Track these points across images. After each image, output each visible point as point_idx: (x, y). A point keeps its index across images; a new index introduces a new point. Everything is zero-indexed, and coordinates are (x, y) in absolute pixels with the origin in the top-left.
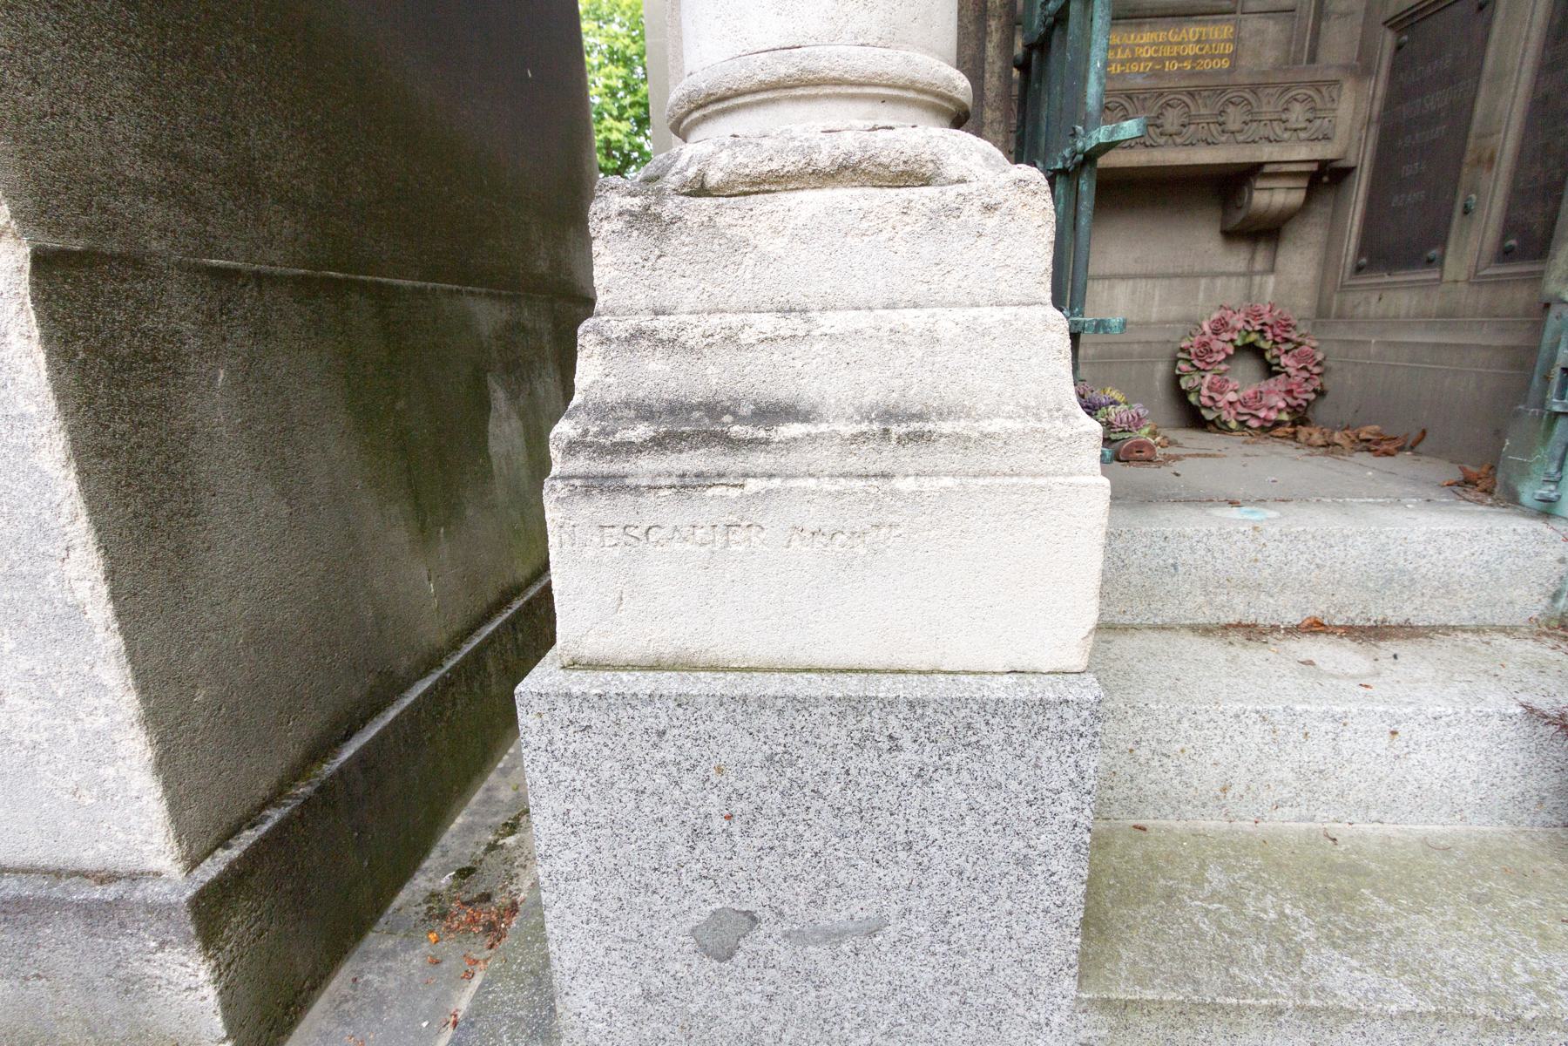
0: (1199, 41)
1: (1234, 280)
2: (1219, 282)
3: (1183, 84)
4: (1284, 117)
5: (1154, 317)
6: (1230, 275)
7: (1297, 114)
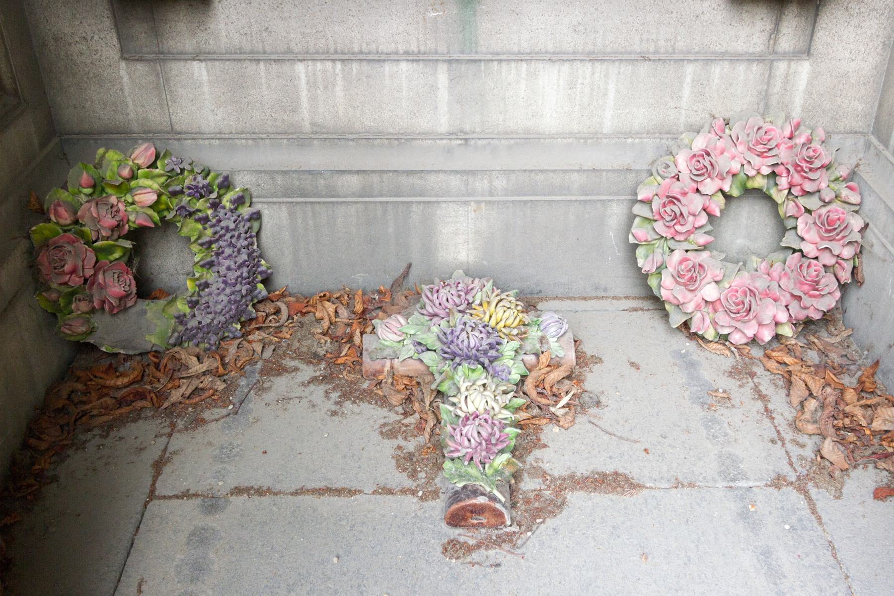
1: (741, 68)
2: (717, 70)
5: (608, 125)
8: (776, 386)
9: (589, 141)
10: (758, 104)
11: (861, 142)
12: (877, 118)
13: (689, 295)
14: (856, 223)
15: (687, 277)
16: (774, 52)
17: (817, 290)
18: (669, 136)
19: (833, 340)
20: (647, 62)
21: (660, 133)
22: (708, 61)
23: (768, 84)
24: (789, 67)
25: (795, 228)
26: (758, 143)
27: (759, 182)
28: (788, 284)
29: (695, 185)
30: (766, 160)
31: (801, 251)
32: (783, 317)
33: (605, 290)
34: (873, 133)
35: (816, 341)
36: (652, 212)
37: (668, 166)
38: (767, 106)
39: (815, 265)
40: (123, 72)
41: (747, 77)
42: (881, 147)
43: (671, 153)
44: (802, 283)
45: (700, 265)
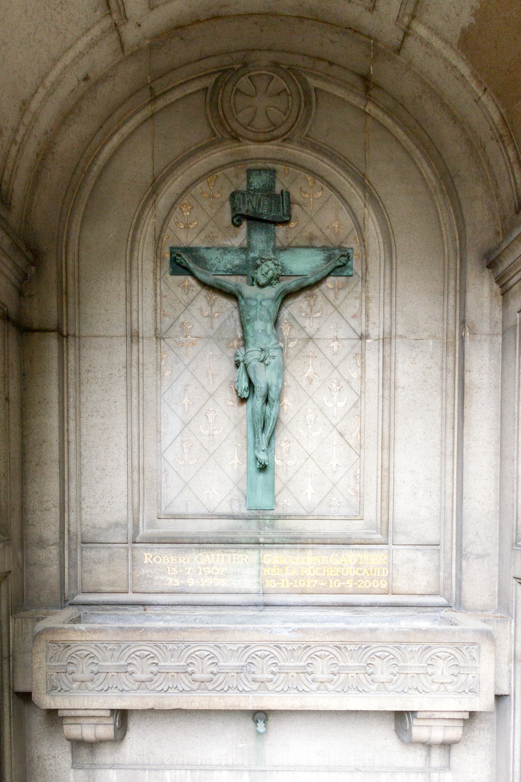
0: (357, 565)
3: (328, 638)
4: (430, 670)
16: (430, 767)
40: (71, 775)
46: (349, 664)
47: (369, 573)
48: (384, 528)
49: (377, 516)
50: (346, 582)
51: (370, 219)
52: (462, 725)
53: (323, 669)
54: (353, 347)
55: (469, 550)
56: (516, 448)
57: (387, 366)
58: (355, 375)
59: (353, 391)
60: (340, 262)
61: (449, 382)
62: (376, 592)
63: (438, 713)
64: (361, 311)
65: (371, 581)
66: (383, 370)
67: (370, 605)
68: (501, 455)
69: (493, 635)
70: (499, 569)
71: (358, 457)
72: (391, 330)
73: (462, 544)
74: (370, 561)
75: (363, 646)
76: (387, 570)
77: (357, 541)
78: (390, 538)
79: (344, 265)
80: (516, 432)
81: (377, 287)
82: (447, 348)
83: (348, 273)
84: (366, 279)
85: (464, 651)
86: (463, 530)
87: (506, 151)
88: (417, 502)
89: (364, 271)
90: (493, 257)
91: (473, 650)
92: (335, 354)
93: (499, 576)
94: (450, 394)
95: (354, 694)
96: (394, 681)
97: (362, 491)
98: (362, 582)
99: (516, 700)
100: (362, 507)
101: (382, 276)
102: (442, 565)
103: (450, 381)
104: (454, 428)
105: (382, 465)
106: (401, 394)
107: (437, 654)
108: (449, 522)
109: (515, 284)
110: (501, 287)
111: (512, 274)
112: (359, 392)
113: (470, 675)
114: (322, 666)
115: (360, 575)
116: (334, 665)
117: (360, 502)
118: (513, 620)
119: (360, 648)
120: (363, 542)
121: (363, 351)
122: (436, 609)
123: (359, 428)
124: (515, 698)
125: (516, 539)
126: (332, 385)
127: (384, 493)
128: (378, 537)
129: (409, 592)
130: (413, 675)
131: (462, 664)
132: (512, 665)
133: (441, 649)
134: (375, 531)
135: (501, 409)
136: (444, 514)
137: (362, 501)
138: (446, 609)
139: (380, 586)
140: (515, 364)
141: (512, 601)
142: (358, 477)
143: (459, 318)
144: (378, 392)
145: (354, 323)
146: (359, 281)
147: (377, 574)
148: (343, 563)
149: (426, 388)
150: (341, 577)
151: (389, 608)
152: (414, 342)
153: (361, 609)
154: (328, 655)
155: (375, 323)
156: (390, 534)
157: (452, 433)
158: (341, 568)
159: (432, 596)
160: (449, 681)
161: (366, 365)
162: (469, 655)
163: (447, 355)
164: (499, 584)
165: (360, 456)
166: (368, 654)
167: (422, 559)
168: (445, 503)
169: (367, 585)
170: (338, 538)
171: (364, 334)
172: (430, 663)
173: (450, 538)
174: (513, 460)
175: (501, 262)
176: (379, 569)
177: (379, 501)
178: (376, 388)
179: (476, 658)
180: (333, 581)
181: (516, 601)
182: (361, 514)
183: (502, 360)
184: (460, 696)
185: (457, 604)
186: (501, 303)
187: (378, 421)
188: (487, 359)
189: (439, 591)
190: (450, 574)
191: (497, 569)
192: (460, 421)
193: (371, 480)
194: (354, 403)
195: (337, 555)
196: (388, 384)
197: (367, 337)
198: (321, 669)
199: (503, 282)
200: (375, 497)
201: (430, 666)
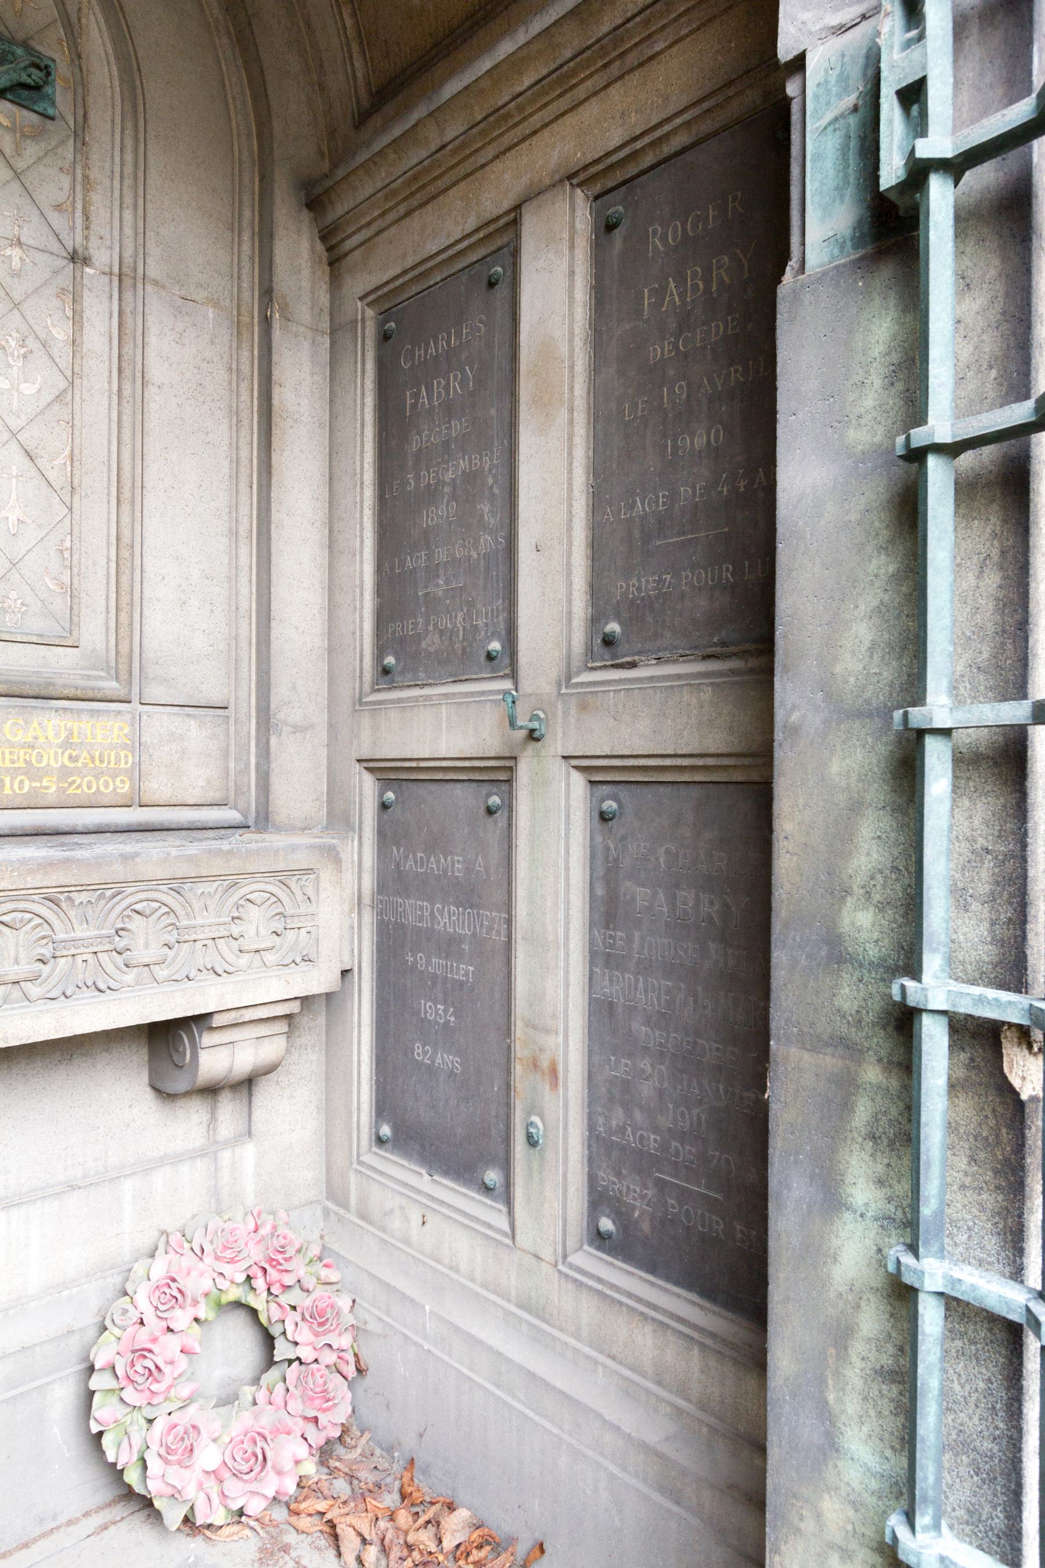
0: (67, 744)
1: (185, 1168)
2: (158, 1178)
3: (31, 881)
4: (235, 930)
6: (175, 1159)
7: (256, 925)
8: (319, 1549)
9: (11, 1312)
10: (209, 1203)
11: (319, 1212)
12: (328, 1182)
13: (186, 1473)
14: (344, 1302)
15: (180, 1451)
16: (216, 1142)
17: (328, 1400)
18: (113, 1271)
19: (355, 1454)
20: (76, 1191)
21: (102, 1271)
22: (147, 1171)
23: (216, 1176)
24: (234, 1154)
25: (284, 1333)
26: (225, 1248)
27: (234, 1294)
28: (296, 1406)
29: (164, 1324)
30: (237, 1265)
31: (298, 1359)
32: (302, 1451)
33: (55, 1517)
34: (327, 1199)
35: (337, 1464)
36: (117, 1378)
37: (125, 1311)
38: (218, 1202)
39: (318, 1370)
41: (192, 1176)
42: (342, 1211)
43: (126, 1294)
44: (312, 1399)
45: (194, 1427)
46: (78, 934)
47: (93, 762)
48: (123, 668)
49: (108, 641)
50: (41, 782)
51: (92, 17)
52: (286, 1029)
53: (18, 953)
54: (56, 273)
55: (281, 716)
56: (358, 534)
57: (127, 334)
58: (61, 333)
59: (55, 368)
60: (29, 76)
61: (243, 399)
62: (106, 801)
63: (250, 1010)
64: (74, 201)
65: (97, 779)
66: (120, 339)
67: (95, 829)
68: (329, 548)
69: (338, 853)
70: (329, 752)
71: (66, 510)
72: (135, 262)
73: (269, 705)
74: (94, 736)
75: (109, 893)
76: (130, 755)
77: (66, 692)
78: (135, 690)
79: (37, 88)
80: (358, 506)
81: (108, 165)
82: (238, 332)
83: (45, 109)
84: (84, 139)
85: (293, 886)
86: (272, 678)
87: (341, 14)
88: (188, 620)
89: (80, 120)
90: (318, 190)
91: (307, 884)
92: (16, 274)
93: (329, 765)
94: (246, 422)
95: (88, 998)
96: (169, 960)
97: (76, 585)
98: (78, 781)
99: (363, 975)
100: (75, 619)
101: (117, 149)
102: (232, 748)
103: (245, 396)
104: (251, 487)
105: (118, 536)
106: (156, 400)
107: (248, 897)
108: (245, 664)
109: (354, 249)
110: (327, 250)
111: (350, 231)
112: (69, 373)
113: (302, 930)
114: (17, 945)
115: (73, 765)
116: (45, 941)
117: (71, 608)
118: (356, 837)
119: (101, 897)
120: (79, 693)
121: (78, 288)
122: (223, 832)
123: (69, 448)
124: (360, 972)
125: (361, 692)
126: (7, 342)
127: (123, 593)
128: (111, 686)
129: (173, 801)
130: (206, 942)
131: (290, 911)
132: (355, 915)
133: (254, 887)
134: (103, 674)
135: (330, 467)
136: (236, 649)
137: (75, 607)
138: (241, 831)
139: (115, 789)
140: (356, 387)
141: (355, 801)
142: (67, 554)
143: (260, 283)
144: (109, 383)
145: (58, 221)
146: (69, 137)
147: (109, 763)
148: (36, 738)
149: (202, 398)
150: (30, 771)
151: (133, 835)
152: (180, 302)
153: (75, 840)
154: (30, 920)
155: (101, 238)
156: (136, 681)
157: (249, 495)
158: (30, 751)
159: (216, 807)
160: (269, 945)
161: (85, 319)
162: (301, 893)
163: (239, 347)
164: (328, 778)
165: (71, 509)
166: (118, 909)
167: (197, 734)
168: (237, 628)
169: (89, 788)
170: (24, 683)
171: (80, 250)
172: (236, 914)
173: (246, 695)
174: (355, 555)
175: (332, 203)
176: (113, 753)
177: (113, 610)
178: (106, 374)
179: (312, 898)
180: (12, 779)
181: (361, 801)
182: (75, 633)
183: (331, 379)
184: (286, 970)
185: (263, 819)
186: (327, 279)
187: (109, 442)
188: (308, 371)
189: (227, 798)
190: (247, 765)
191: (324, 752)
192: (264, 474)
193: (94, 564)
194: (57, 394)
195: (21, 722)
196: (129, 371)
197: (86, 261)
198: (12, 954)
199: (334, 242)
200: (104, 602)
201: (236, 921)
